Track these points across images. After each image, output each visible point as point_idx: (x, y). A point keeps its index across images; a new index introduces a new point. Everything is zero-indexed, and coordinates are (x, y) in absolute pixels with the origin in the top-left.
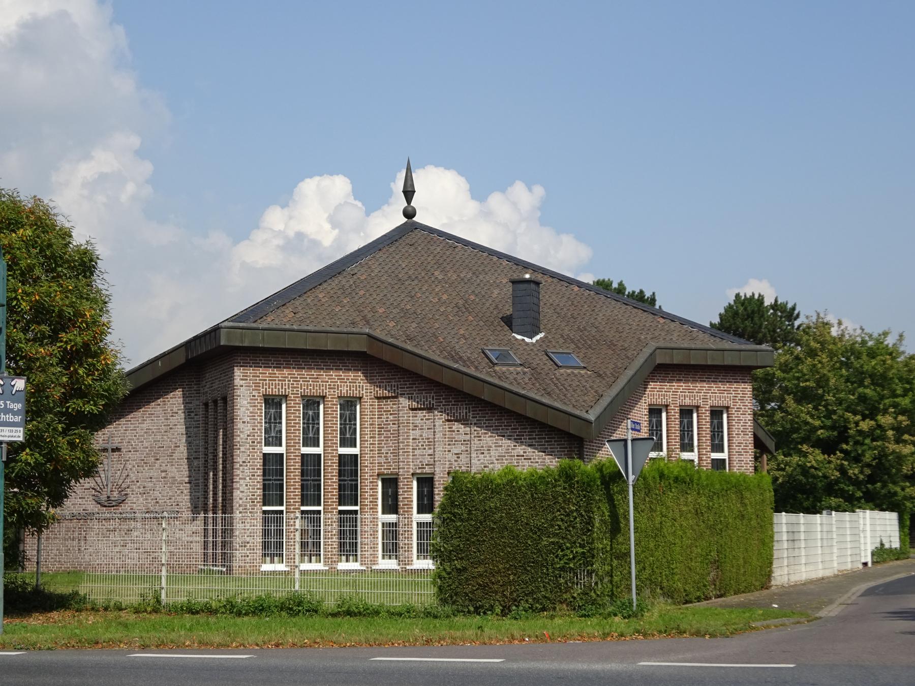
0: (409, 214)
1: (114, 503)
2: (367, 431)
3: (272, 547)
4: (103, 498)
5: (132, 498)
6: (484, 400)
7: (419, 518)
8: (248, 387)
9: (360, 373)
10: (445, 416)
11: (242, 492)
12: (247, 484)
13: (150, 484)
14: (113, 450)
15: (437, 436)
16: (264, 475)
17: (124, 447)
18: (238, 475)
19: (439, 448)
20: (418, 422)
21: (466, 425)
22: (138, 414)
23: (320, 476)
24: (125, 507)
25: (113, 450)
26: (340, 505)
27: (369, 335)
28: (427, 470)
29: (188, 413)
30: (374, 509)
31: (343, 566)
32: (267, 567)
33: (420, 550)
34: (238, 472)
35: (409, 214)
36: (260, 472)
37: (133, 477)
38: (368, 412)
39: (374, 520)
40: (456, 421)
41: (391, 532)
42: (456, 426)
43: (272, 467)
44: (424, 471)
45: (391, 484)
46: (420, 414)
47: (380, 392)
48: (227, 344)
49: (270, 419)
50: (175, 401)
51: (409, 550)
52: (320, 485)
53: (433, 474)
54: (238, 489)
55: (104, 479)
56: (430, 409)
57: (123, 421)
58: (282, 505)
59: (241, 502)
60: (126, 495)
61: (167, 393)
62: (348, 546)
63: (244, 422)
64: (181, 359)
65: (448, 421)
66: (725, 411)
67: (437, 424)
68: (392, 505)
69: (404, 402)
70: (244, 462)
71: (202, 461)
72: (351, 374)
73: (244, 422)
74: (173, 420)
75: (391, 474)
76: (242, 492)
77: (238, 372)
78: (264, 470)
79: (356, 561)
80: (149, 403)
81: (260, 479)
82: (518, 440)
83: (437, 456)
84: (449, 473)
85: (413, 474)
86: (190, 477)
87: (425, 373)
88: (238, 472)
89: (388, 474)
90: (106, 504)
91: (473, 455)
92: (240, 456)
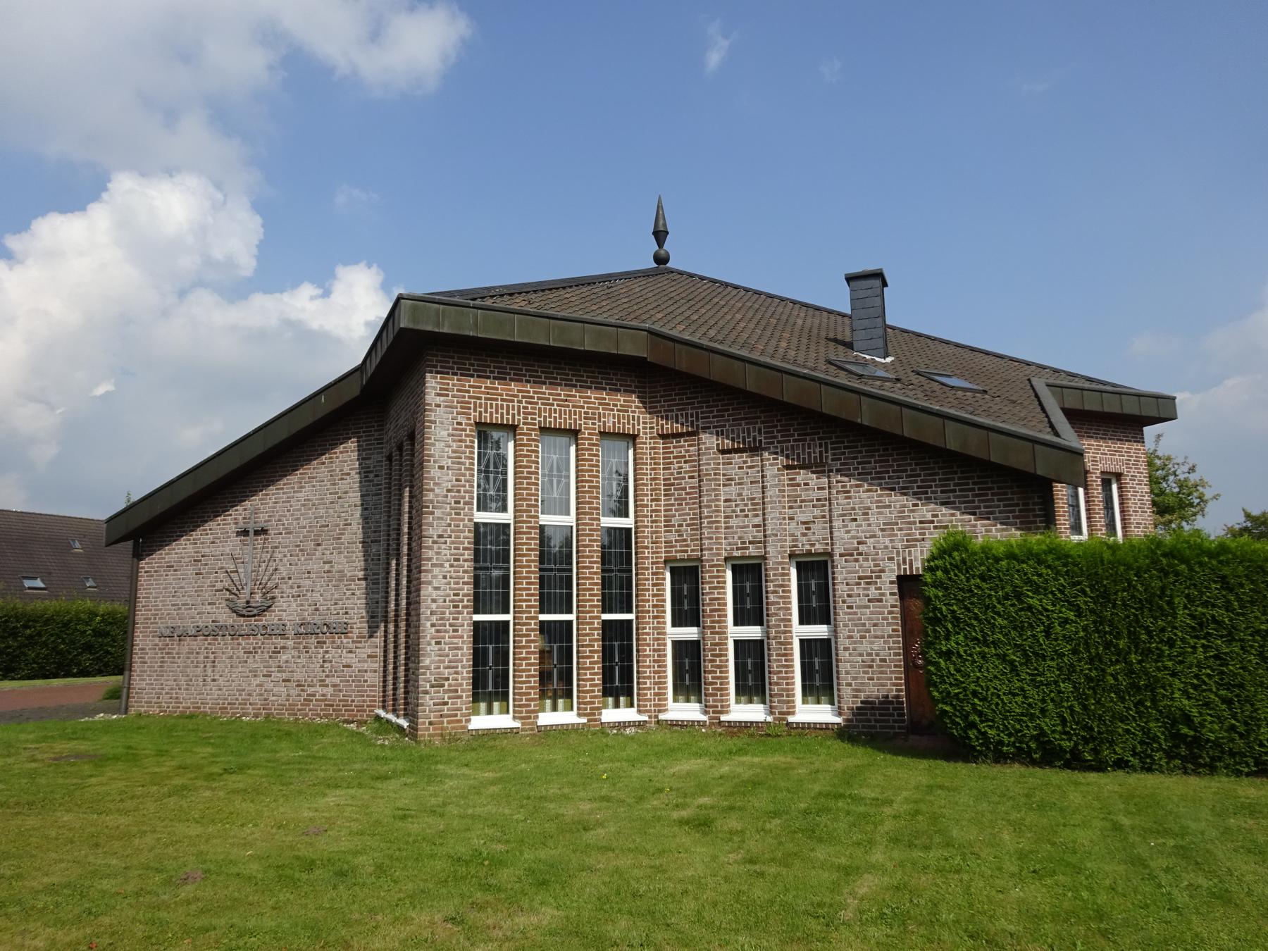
0: (661, 260)
1: (255, 612)
2: (647, 490)
3: (489, 682)
4: (241, 603)
5: (281, 603)
6: (861, 426)
7: (801, 631)
8: (448, 409)
9: (634, 398)
10: (782, 460)
11: (437, 589)
12: (445, 579)
13: (308, 582)
14: (257, 533)
15: (768, 494)
16: (476, 560)
17: (268, 526)
18: (429, 559)
19: (773, 515)
20: (734, 471)
21: (820, 473)
22: (293, 479)
23: (571, 564)
24: (270, 618)
25: (257, 533)
26: (542, 612)
27: (651, 332)
28: (752, 551)
29: (365, 473)
30: (659, 617)
31: (610, 715)
32: (481, 722)
33: (739, 691)
34: (430, 554)
35: (661, 260)
36: (469, 555)
37: (283, 571)
38: (647, 459)
39: (660, 639)
40: (801, 468)
41: (688, 655)
42: (802, 476)
43: (490, 547)
44: (747, 553)
45: (687, 577)
46: (736, 458)
47: (668, 427)
48: (411, 326)
49: (487, 466)
50: (346, 457)
51: (723, 689)
52: (571, 577)
53: (764, 558)
54: (429, 583)
55: (242, 575)
56: (755, 450)
57: (272, 489)
58: (507, 612)
59: (434, 606)
60: (273, 598)
61: (335, 446)
62: (618, 683)
63: (441, 468)
64: (354, 391)
65: (788, 467)
66: (1114, 481)
67: (768, 473)
68: (687, 611)
69: (710, 440)
70: (440, 536)
71: (383, 545)
72: (620, 398)
73: (441, 468)
74: (343, 486)
75: (689, 559)
76: (437, 589)
77: (432, 383)
78: (477, 552)
79: (632, 705)
80: (309, 461)
81: (469, 566)
82: (922, 494)
83: (769, 527)
84: (791, 556)
85: (726, 559)
86: (366, 570)
87: (751, 386)
88: (430, 554)
89: (682, 560)
90: (244, 612)
91: (836, 524)
92: (434, 526)
